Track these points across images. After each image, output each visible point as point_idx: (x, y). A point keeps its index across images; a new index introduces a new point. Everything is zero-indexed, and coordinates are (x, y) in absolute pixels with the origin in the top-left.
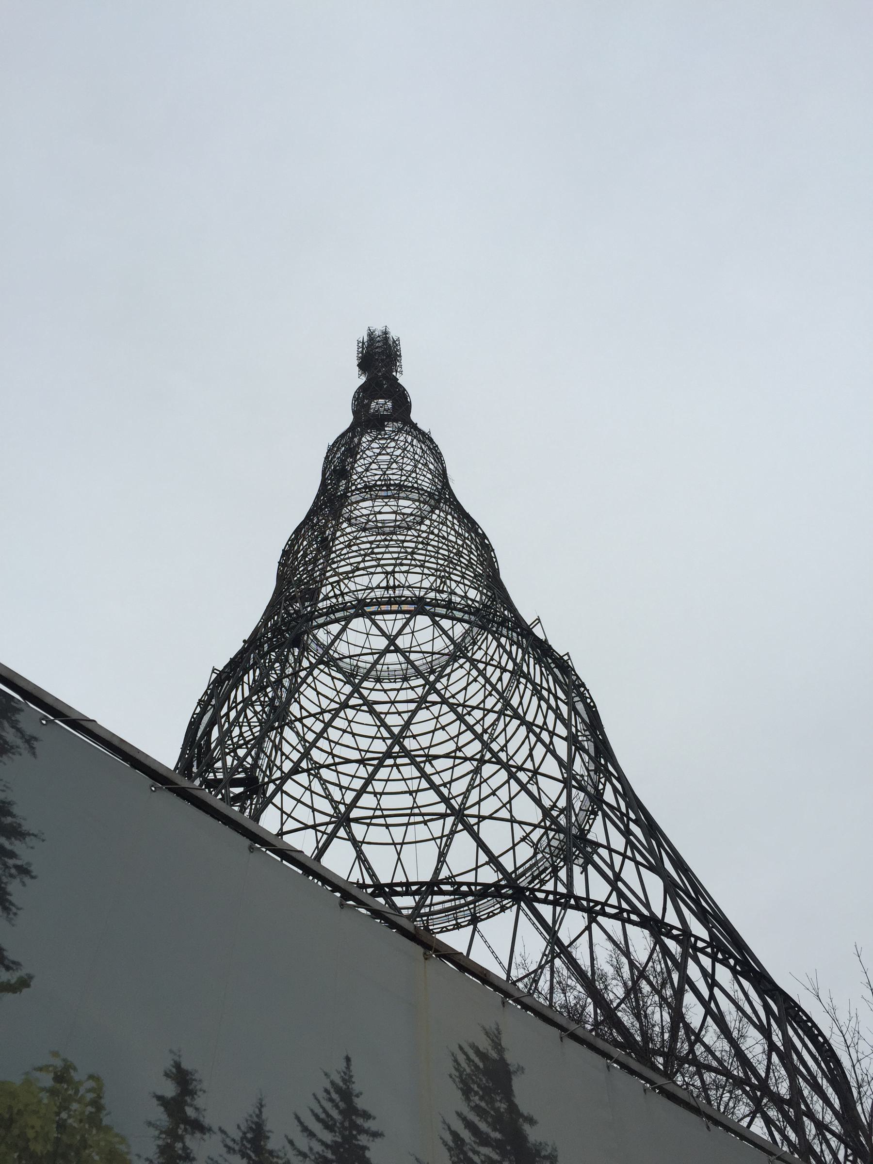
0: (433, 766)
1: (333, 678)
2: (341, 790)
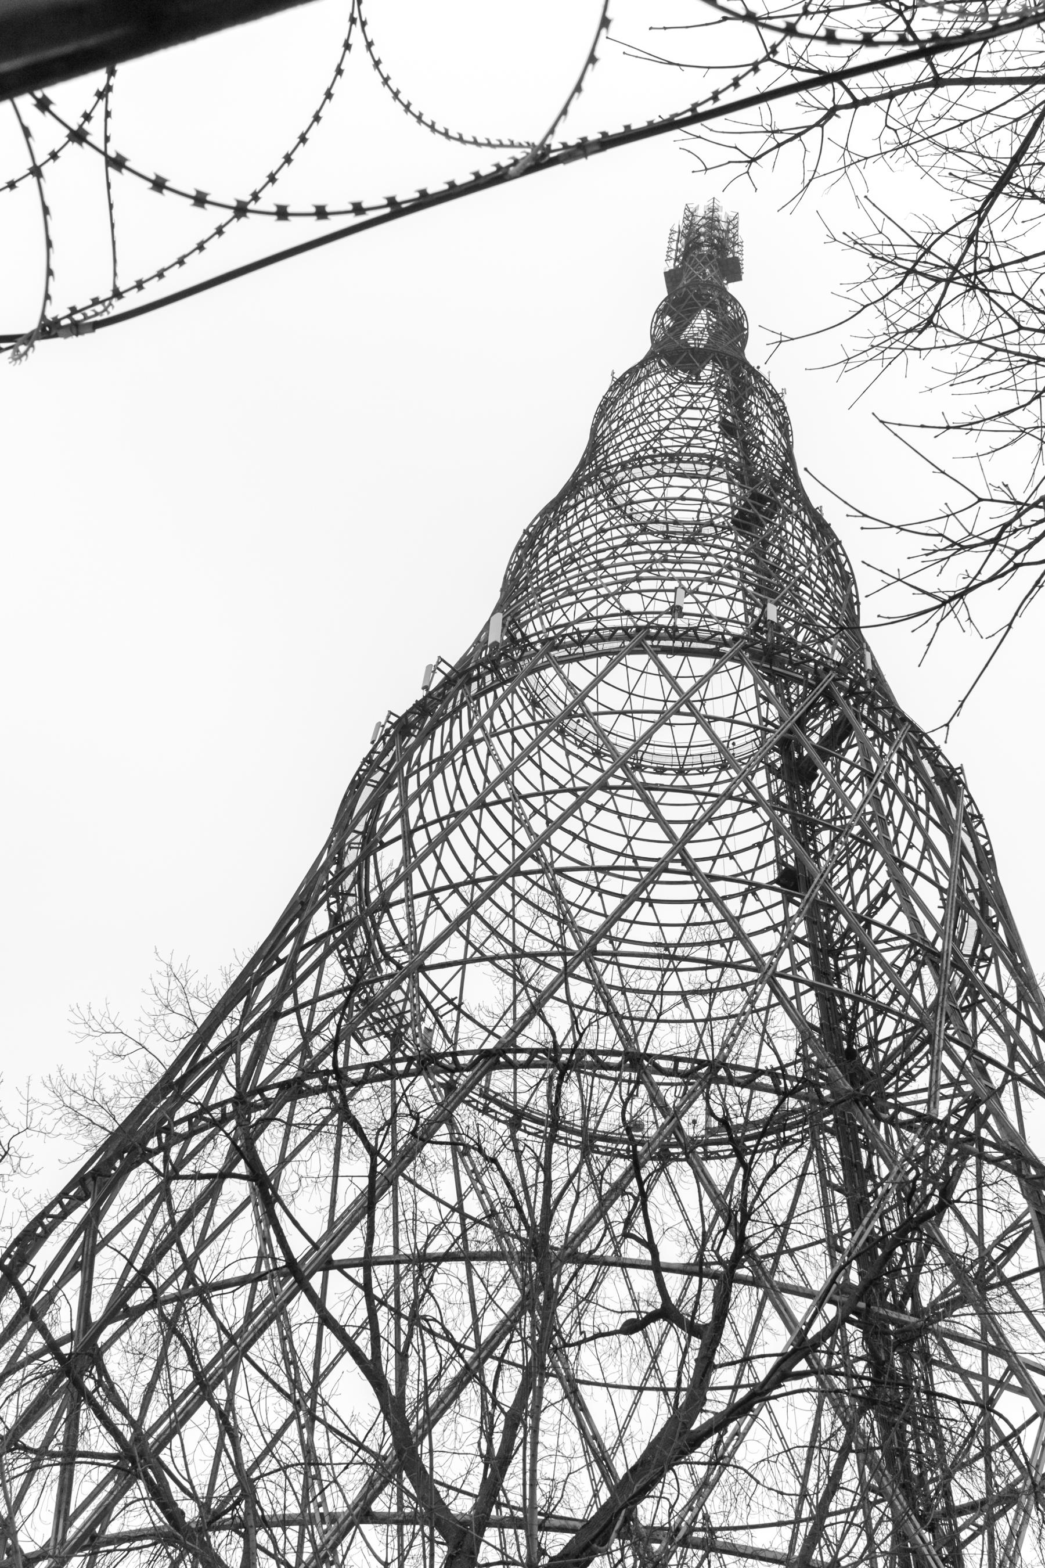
0: (758, 900)
1: (568, 753)
2: (513, 896)
